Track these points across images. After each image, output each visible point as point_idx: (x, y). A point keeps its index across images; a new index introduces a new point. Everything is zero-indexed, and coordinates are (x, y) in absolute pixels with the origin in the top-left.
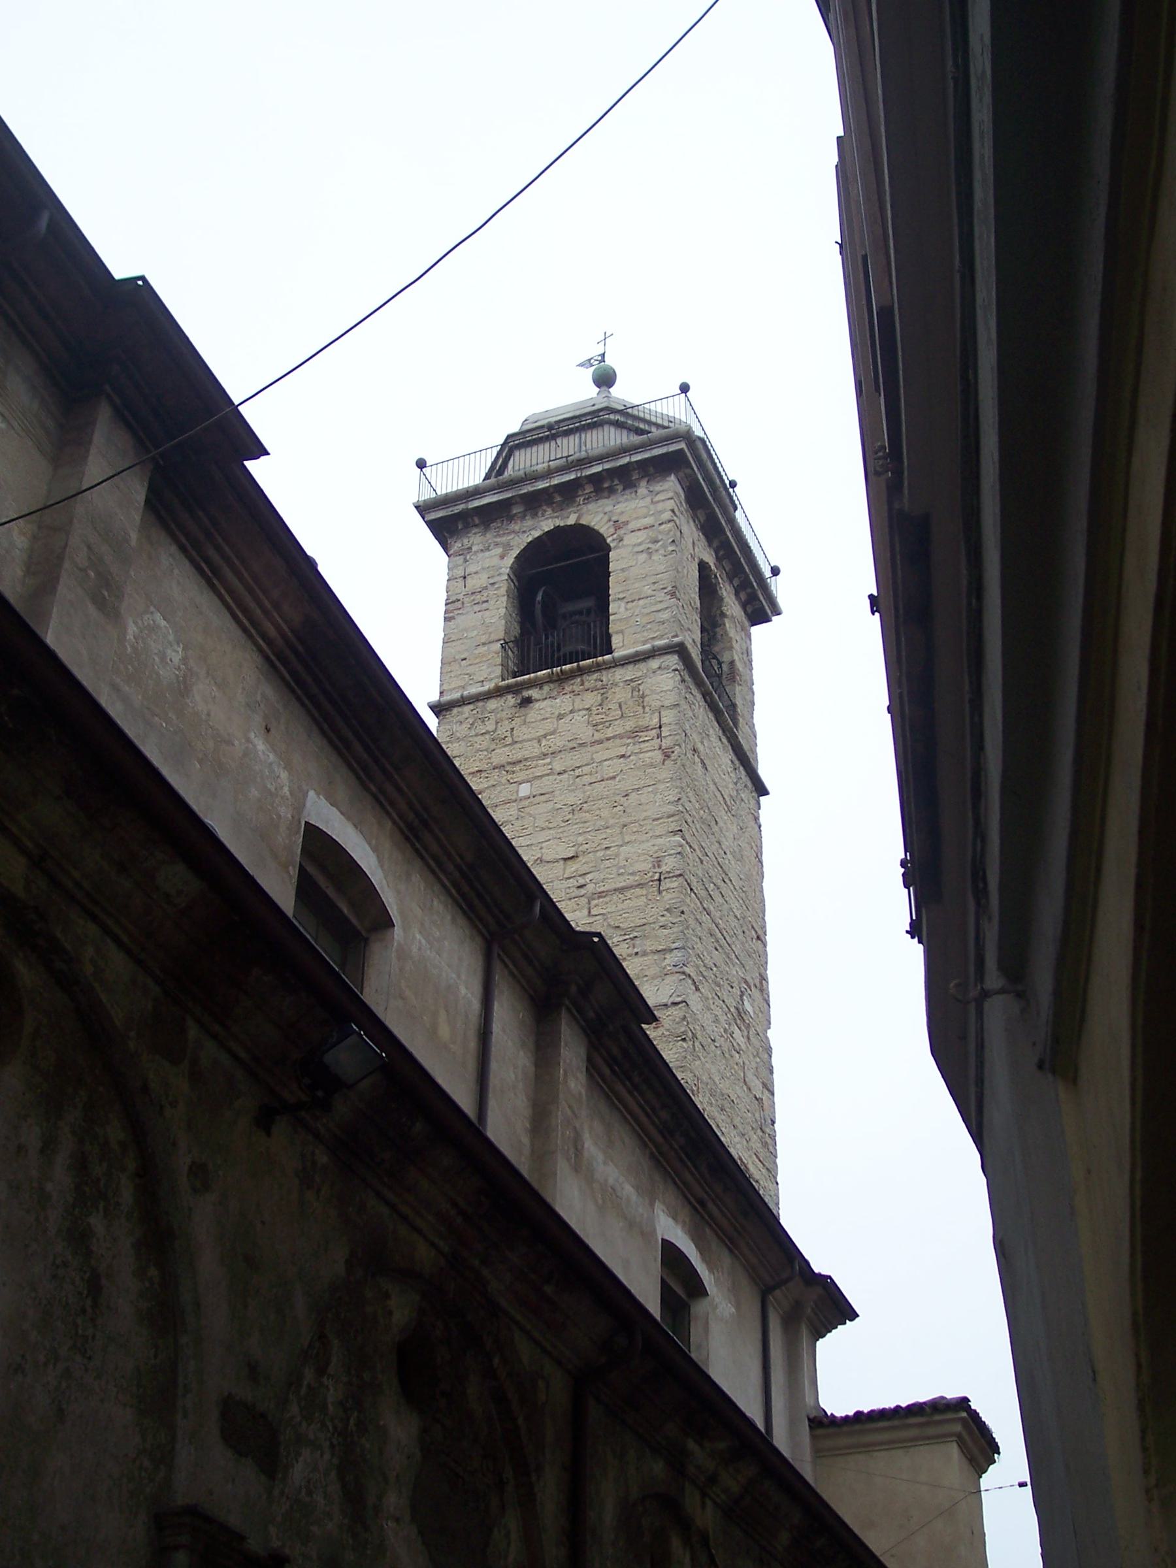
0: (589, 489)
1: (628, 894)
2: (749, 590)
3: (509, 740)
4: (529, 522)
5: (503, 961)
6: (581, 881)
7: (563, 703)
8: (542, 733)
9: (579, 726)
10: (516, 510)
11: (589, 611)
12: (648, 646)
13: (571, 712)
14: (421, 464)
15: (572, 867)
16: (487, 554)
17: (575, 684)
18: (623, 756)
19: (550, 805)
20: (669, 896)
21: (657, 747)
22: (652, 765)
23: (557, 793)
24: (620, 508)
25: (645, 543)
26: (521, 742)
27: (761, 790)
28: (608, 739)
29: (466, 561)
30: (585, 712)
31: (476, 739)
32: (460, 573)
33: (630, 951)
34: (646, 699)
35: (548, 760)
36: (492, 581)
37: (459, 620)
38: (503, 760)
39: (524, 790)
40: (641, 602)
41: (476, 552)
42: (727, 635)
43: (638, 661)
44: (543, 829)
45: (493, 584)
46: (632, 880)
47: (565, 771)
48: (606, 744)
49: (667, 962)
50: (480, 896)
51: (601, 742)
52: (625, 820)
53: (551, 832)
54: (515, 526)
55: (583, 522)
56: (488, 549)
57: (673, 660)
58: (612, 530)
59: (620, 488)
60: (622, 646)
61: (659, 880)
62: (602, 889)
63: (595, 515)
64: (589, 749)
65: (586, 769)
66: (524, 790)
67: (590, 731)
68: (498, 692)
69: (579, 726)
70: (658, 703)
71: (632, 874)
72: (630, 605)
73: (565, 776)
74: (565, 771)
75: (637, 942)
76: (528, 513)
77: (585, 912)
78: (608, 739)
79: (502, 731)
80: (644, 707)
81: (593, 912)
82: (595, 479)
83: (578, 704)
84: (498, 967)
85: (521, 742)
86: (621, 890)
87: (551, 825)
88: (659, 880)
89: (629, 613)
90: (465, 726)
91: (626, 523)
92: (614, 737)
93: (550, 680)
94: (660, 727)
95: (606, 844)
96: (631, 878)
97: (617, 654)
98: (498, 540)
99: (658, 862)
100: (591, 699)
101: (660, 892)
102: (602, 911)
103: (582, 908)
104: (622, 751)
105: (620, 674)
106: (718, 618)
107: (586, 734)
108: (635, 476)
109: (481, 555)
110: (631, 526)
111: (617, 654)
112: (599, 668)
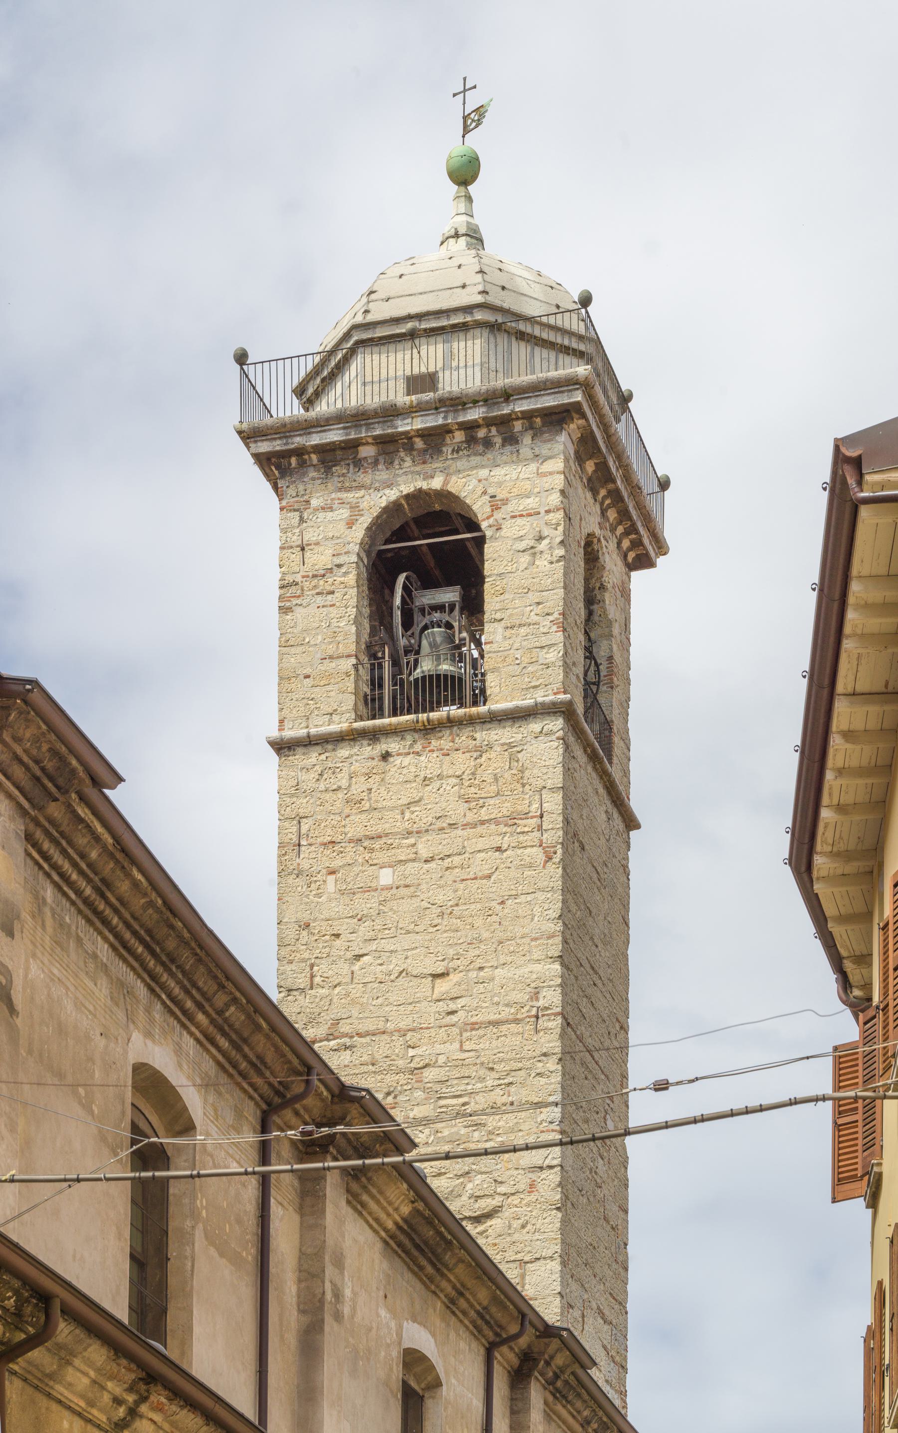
0: (459, 436)
1: (504, 1028)
2: (634, 536)
4: (383, 475)
6: (452, 1006)
8: (404, 801)
9: (446, 800)
11: (452, 607)
12: (529, 702)
14: (241, 358)
15: (442, 986)
16: (330, 515)
17: (443, 741)
18: (498, 849)
19: (416, 902)
20: (548, 1037)
21: (537, 843)
22: (530, 866)
23: (424, 887)
24: (499, 472)
25: (519, 503)
27: (631, 823)
28: (483, 823)
29: (302, 520)
30: (454, 781)
31: (327, 796)
32: (295, 540)
33: (505, 1099)
34: (527, 774)
35: (412, 841)
36: (338, 561)
37: (299, 612)
38: (360, 832)
39: (386, 877)
40: (523, 631)
41: (316, 510)
42: (606, 615)
43: (519, 718)
44: (408, 932)
45: (339, 566)
46: (507, 1013)
47: (432, 859)
48: (480, 829)
49: (543, 1117)
50: (487, 1323)
51: (474, 826)
52: (500, 935)
53: (418, 937)
54: (365, 478)
55: (452, 488)
56: (331, 509)
57: (557, 724)
58: (488, 509)
59: (498, 440)
62: (474, 1019)
63: (471, 482)
64: (459, 832)
65: (457, 860)
67: (463, 807)
69: (446, 800)
70: (540, 783)
71: (507, 1005)
72: (509, 631)
73: (433, 865)
74: (432, 859)
75: (512, 1089)
77: (457, 1045)
78: (483, 823)
79: (359, 787)
80: (523, 785)
81: (465, 1047)
82: (470, 428)
83: (447, 770)
86: (496, 1023)
87: (417, 929)
88: (537, 1017)
89: (506, 644)
90: (313, 775)
92: (489, 821)
93: (414, 729)
94: (541, 816)
95: (479, 963)
96: (507, 1009)
99: (536, 996)
100: (462, 762)
101: (537, 1031)
102: (474, 1047)
103: (453, 1041)
104: (497, 841)
106: (596, 592)
107: (458, 811)
108: (518, 426)
109: (321, 515)
110: (510, 507)
112: (471, 721)
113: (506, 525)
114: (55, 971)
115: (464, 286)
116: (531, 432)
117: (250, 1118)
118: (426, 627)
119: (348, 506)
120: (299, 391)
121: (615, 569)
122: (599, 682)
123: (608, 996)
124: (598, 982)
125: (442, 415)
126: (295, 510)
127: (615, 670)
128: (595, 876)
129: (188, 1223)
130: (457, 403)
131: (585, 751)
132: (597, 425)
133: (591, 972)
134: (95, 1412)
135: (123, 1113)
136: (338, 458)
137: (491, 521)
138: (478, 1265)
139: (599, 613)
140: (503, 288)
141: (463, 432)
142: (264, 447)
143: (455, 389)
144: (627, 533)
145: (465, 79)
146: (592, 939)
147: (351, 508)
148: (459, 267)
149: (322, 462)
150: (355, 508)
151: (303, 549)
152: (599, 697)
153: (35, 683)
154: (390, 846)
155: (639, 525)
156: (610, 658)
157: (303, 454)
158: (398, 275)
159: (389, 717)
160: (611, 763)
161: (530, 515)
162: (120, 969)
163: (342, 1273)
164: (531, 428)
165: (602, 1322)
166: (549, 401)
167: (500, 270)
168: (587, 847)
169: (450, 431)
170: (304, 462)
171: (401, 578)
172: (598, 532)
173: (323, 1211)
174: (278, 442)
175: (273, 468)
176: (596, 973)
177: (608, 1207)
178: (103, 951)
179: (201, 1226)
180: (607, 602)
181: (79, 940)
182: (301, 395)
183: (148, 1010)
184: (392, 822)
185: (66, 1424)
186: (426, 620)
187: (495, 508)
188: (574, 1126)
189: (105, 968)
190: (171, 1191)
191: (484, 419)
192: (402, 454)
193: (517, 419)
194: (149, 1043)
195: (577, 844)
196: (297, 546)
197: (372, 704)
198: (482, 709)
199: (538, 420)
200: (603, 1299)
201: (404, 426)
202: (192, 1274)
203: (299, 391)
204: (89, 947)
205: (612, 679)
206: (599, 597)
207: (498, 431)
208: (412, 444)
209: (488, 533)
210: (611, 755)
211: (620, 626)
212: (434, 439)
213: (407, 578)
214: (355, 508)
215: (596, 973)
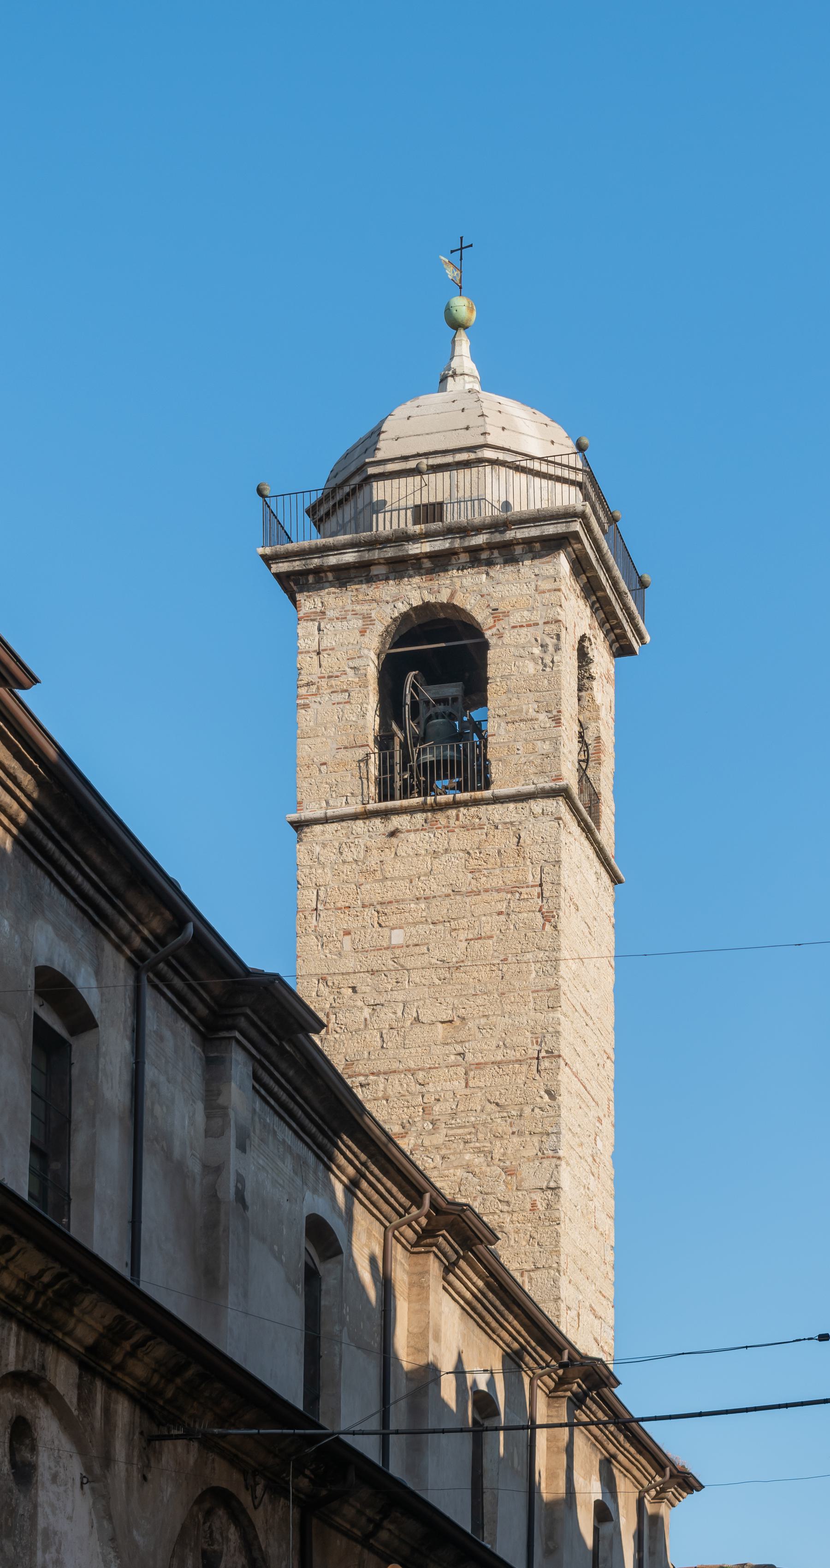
0: (464, 558)
3: (378, 875)
5: (155, 987)
7: (437, 839)
9: (452, 867)
10: (375, 570)
11: (455, 699)
13: (446, 851)
26: (392, 879)
60: (503, 783)
61: (538, 1058)
63: (466, 590)
66: (398, 937)
68: (367, 815)
69: (452, 867)
76: (391, 576)
79: (373, 861)
81: (471, 1084)
82: (474, 552)
84: (150, 997)
85: (392, 879)
91: (506, 614)
97: (497, 790)
98: (358, 608)
105: (496, 812)
107: (465, 881)
108: (518, 550)
111: (497, 790)
112: (476, 802)
113: (507, 634)
114: (261, 1162)
115: (467, 428)
116: (531, 555)
117: (377, 1235)
118: (430, 718)
119: (361, 617)
120: (312, 511)
121: (601, 660)
122: (588, 760)
123: (597, 1032)
124: (590, 1023)
125: (449, 541)
126: (312, 620)
127: (602, 748)
128: (586, 931)
129: (337, 1328)
130: (463, 531)
131: (579, 825)
132: (597, 560)
133: (584, 1014)
134: (355, 1530)
135: (300, 1255)
136: (352, 575)
137: (494, 630)
138: (501, 1286)
139: (588, 698)
140: (503, 429)
141: (467, 554)
142: (283, 567)
143: (463, 519)
144: (612, 629)
145: (461, 238)
146: (584, 986)
147: (364, 618)
148: (463, 410)
149: (337, 579)
150: (367, 618)
151: (319, 653)
152: (588, 772)
153: (277, 977)
154: (402, 911)
155: (624, 622)
156: (598, 738)
157: (320, 572)
158: (406, 417)
159: (400, 799)
160: (599, 829)
161: (529, 626)
162: (300, 1148)
163: (440, 1345)
164: (531, 551)
165: (592, 1317)
166: (550, 529)
167: (500, 412)
168: (580, 908)
169: (456, 554)
170: (321, 578)
171: (411, 677)
172: (589, 633)
173: (428, 1299)
174: (298, 563)
175: (292, 584)
176: (588, 1014)
177: (597, 1216)
178: (288, 1136)
179: (345, 1328)
180: (595, 690)
181: (275, 1133)
182: (313, 515)
183: (315, 1173)
184: (401, 889)
185: (338, 1542)
186: (432, 711)
187: (497, 619)
188: (571, 1151)
189: (289, 1149)
190: (323, 1303)
191: (487, 544)
192: (411, 572)
193: (518, 544)
194: (316, 1197)
195: (572, 907)
196: (314, 651)
197: (386, 793)
198: (487, 794)
199: (538, 545)
200: (594, 1298)
201: (414, 549)
202: (340, 1369)
203: (312, 511)
204: (280, 1136)
205: (599, 757)
206: (587, 686)
207: (499, 553)
208: (420, 564)
209: (492, 641)
210: (599, 823)
211: (606, 709)
212: (440, 562)
213: (415, 677)
214: (367, 618)
215: (588, 1014)
